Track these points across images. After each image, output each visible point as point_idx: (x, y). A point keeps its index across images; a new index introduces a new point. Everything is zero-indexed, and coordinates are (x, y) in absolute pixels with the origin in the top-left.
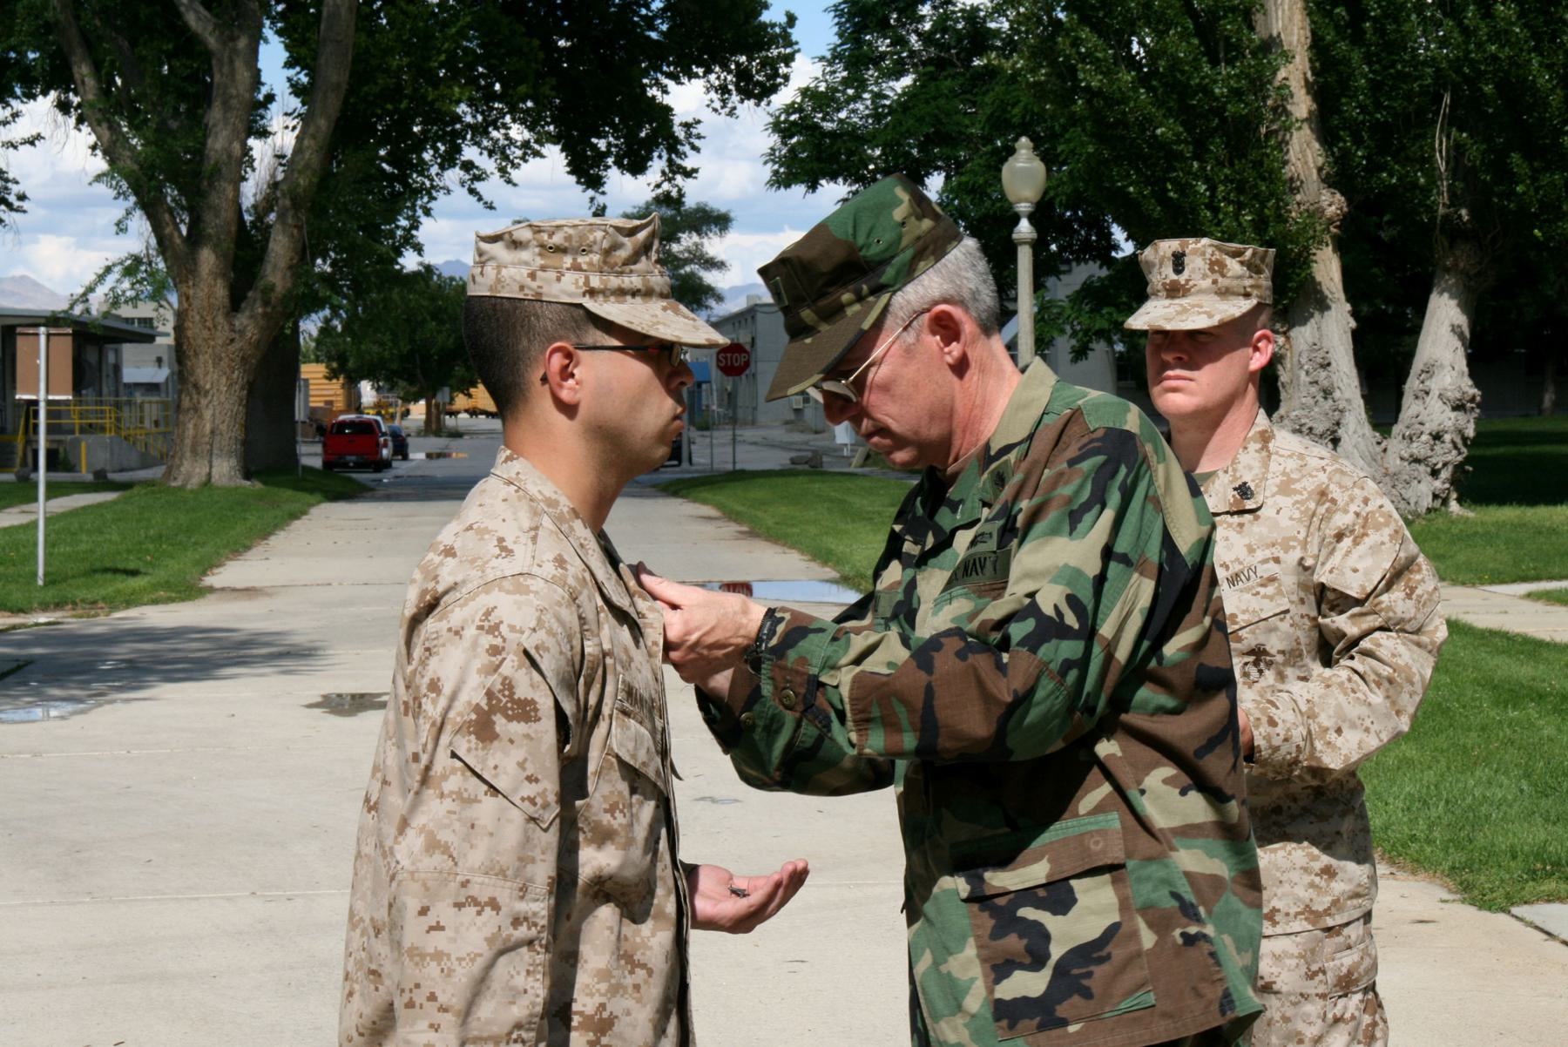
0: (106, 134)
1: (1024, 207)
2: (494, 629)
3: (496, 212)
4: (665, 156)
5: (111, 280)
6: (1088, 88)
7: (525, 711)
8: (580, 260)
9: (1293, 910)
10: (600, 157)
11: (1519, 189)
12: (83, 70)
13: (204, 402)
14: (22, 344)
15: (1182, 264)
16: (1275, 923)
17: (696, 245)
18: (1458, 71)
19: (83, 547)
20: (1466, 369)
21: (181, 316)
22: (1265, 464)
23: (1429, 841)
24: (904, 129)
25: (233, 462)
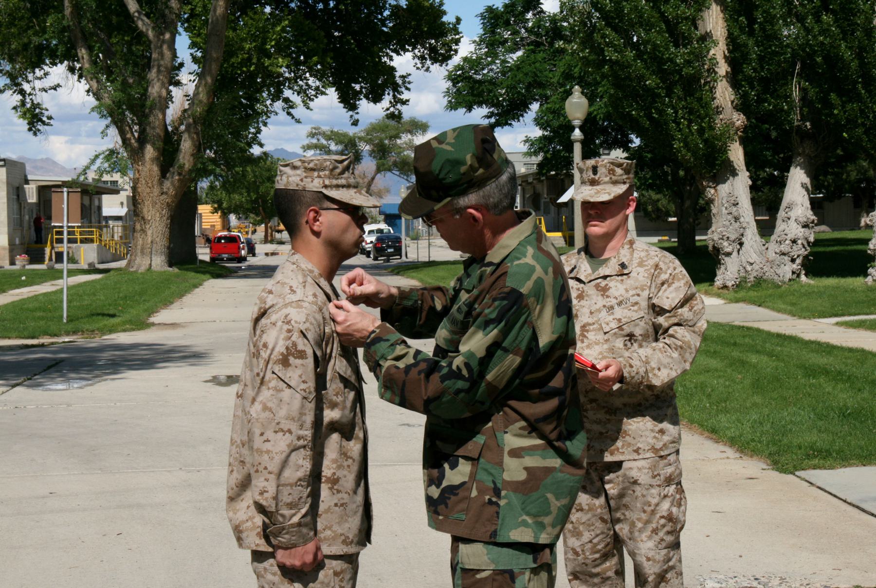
0: (95, 85)
1: (577, 123)
2: (289, 323)
3: (298, 128)
4: (391, 93)
5: (99, 162)
6: (610, 60)
7: (301, 355)
8: (321, 173)
9: (647, 448)
11: (836, 112)
12: (83, 52)
14: (55, 197)
16: (639, 454)
17: (410, 140)
18: (804, 50)
19: (86, 302)
20: (809, 206)
23: (760, 442)
24: (517, 79)
25: (163, 258)
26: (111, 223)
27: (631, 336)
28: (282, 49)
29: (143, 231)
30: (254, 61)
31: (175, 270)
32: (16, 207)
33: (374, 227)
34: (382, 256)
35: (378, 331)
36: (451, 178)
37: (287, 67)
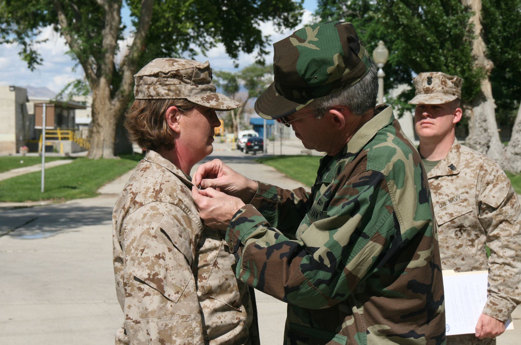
5: (70, 89)
6: (403, 24)
10: (237, 48)
12: (62, 17)
13: (101, 130)
15: (431, 81)
21: (94, 100)
22: (459, 157)
26: (81, 128)
27: (461, 228)
28: (189, 17)
29: (98, 132)
30: (172, 24)
31: (118, 158)
32: (20, 116)
33: (247, 132)
34: (251, 151)
35: (244, 211)
36: (317, 78)
37: (193, 29)
